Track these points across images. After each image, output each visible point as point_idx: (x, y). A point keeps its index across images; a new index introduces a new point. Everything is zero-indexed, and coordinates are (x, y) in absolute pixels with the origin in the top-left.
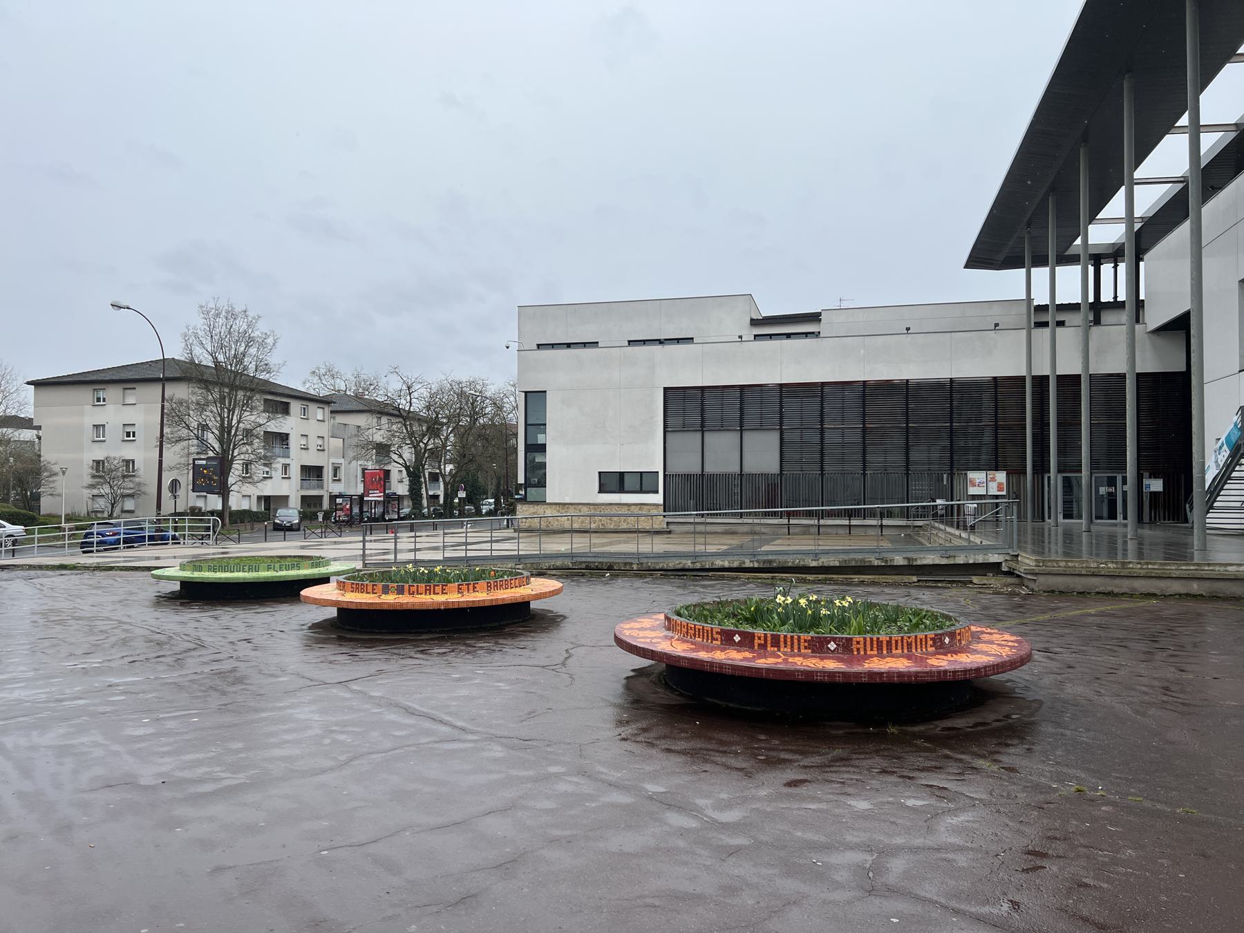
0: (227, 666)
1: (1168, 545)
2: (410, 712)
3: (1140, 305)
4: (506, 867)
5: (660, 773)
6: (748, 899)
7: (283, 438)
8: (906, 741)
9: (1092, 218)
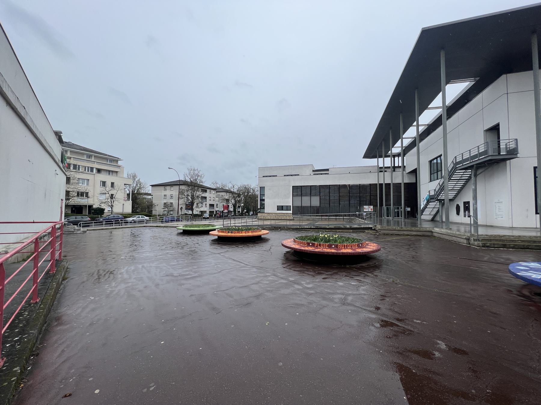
0: (193, 249)
1: (411, 223)
2: (234, 260)
3: (405, 167)
4: (257, 297)
5: (293, 275)
6: (314, 306)
7: (205, 198)
8: (351, 269)
9: (393, 147)
